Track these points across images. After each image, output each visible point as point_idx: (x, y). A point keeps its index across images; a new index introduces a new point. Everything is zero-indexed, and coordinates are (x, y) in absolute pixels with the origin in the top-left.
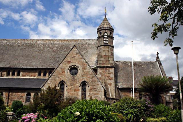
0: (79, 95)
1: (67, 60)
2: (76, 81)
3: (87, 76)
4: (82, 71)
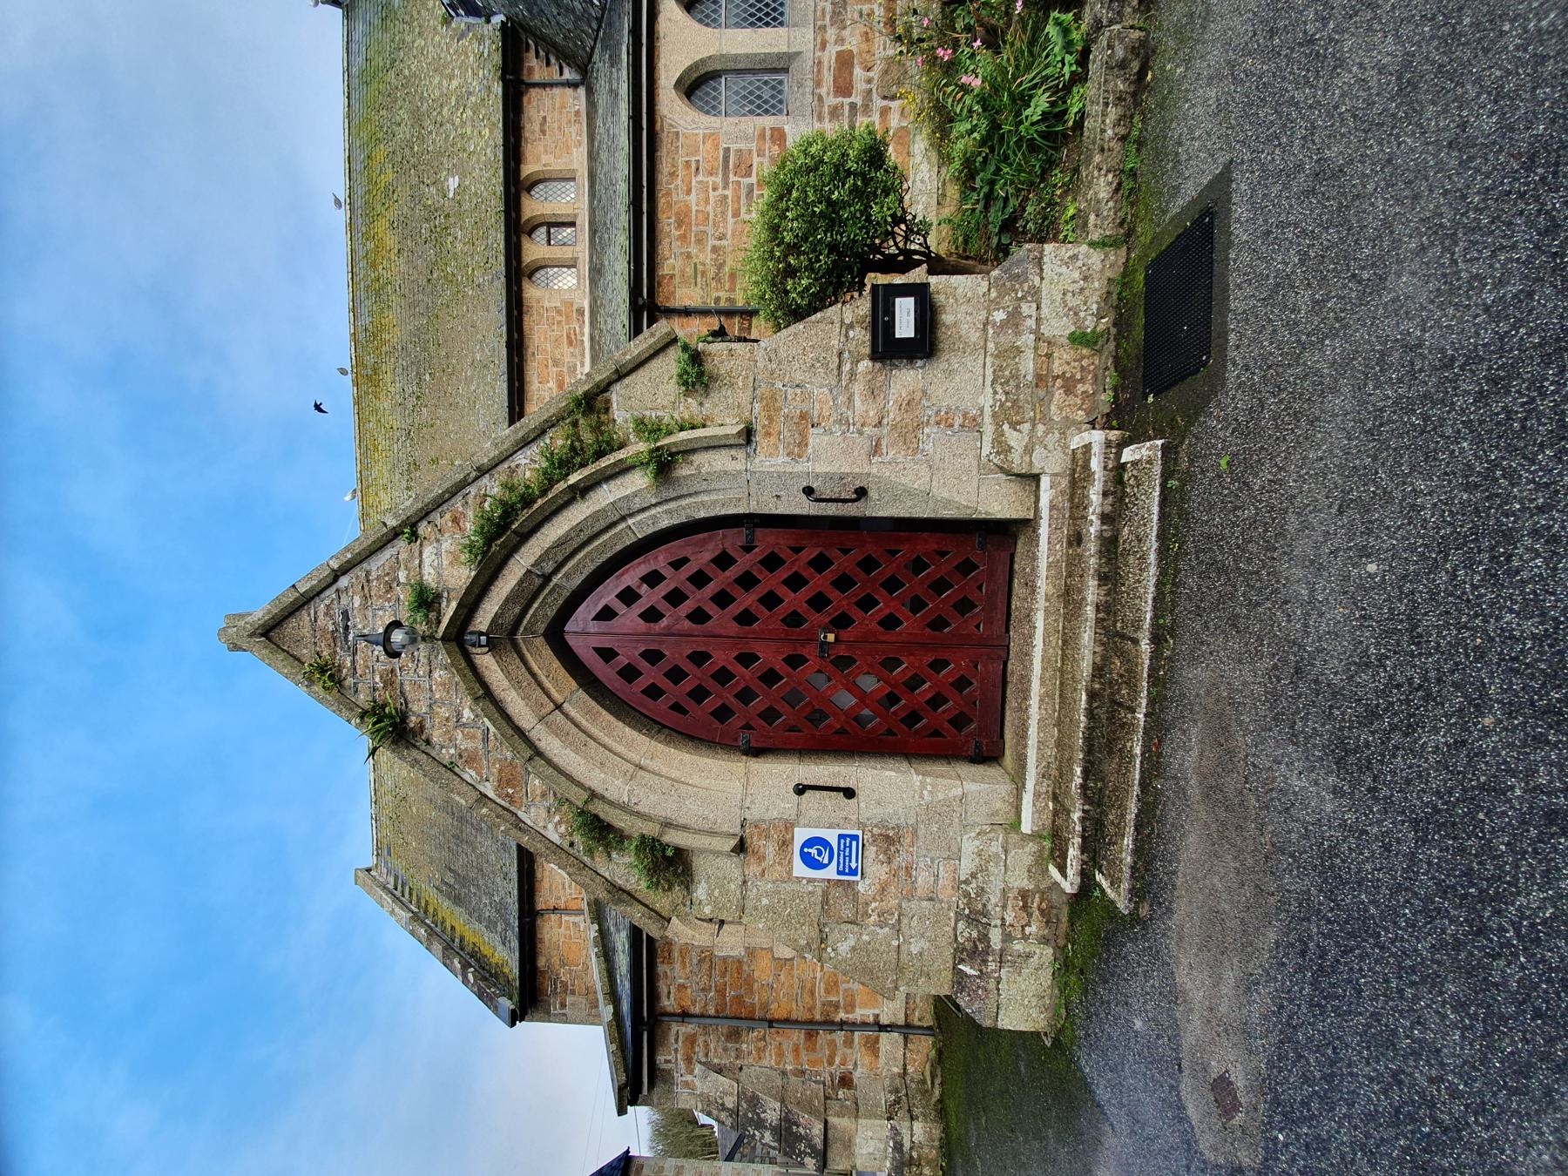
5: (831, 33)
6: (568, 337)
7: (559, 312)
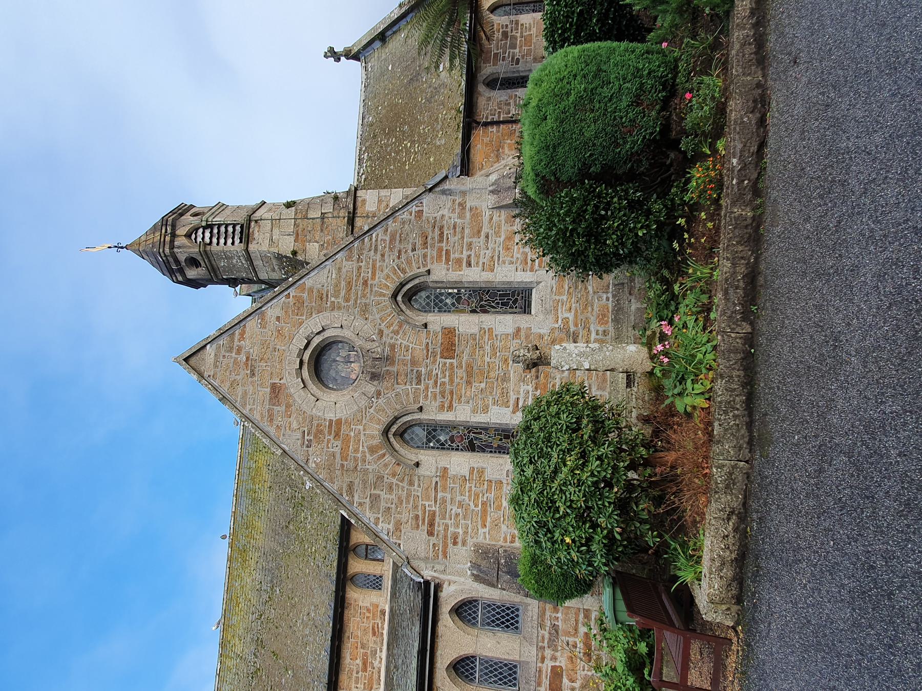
0: (498, 269)
1: (267, 402)
2: (392, 347)
3: (365, 283)
4: (335, 313)
5: (548, 653)
6: (373, 629)
7: (368, 610)
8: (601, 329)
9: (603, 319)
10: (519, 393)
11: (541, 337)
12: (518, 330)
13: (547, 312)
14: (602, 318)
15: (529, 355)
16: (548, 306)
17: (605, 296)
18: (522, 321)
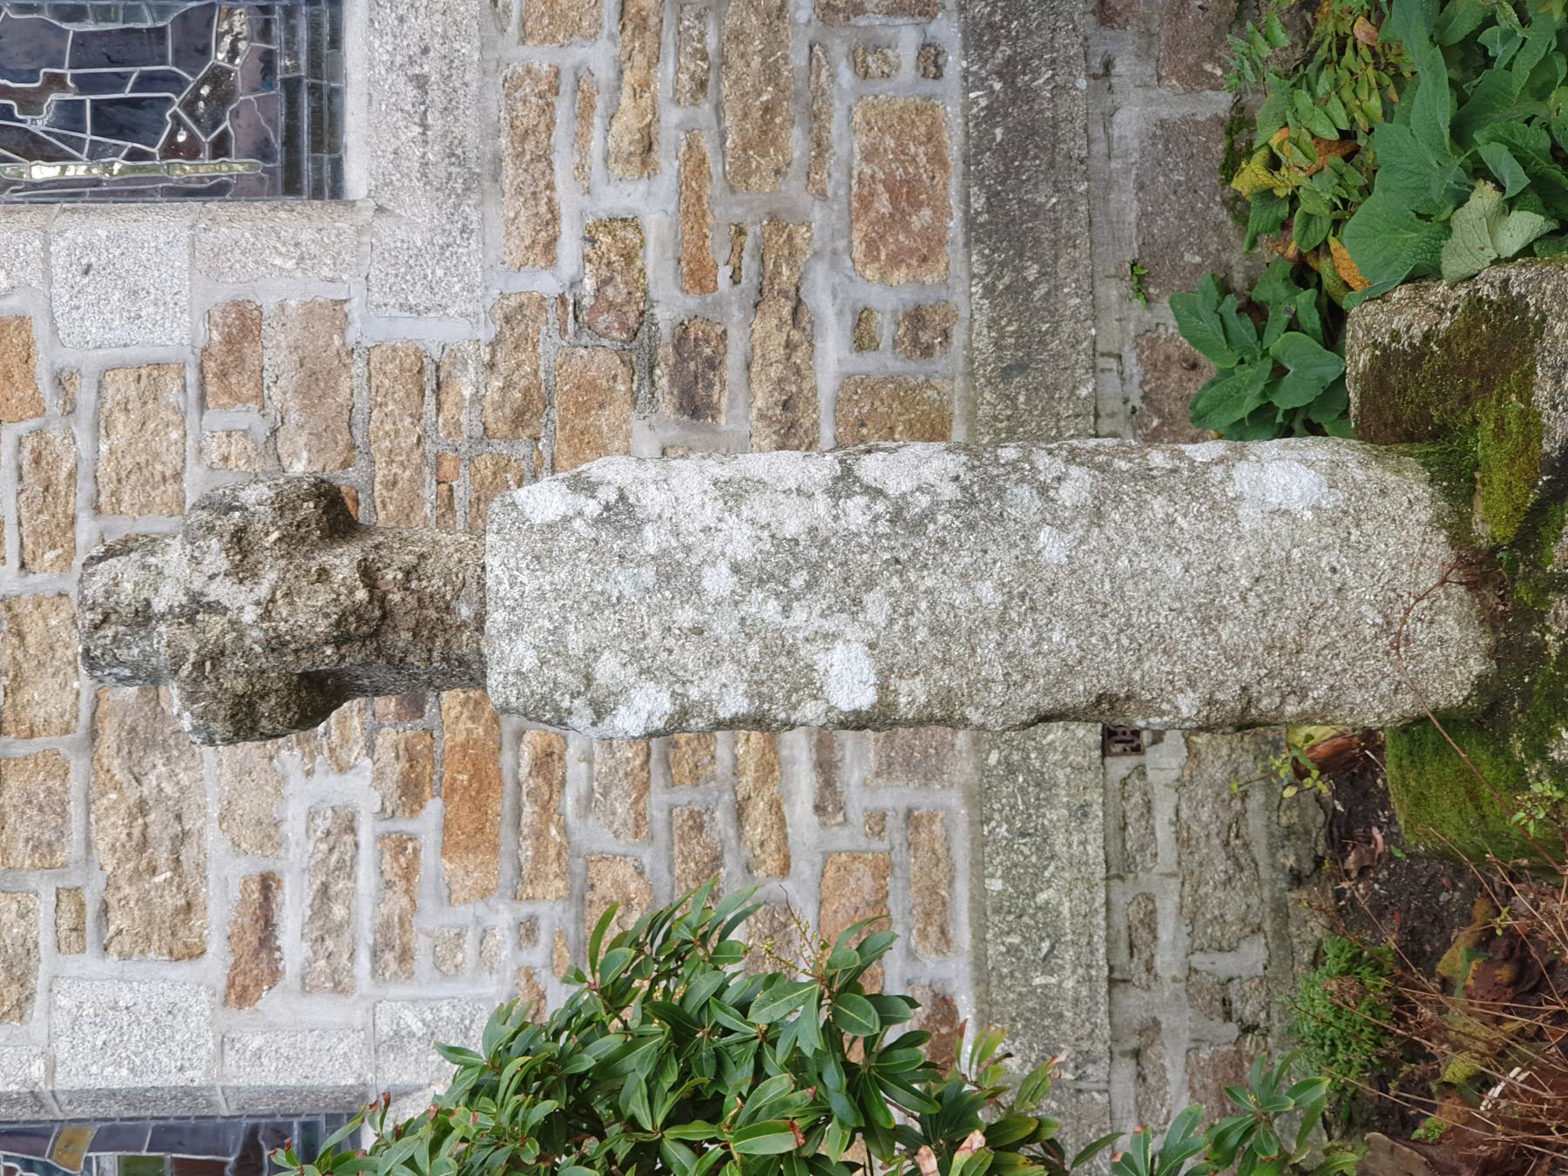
8: (889, 296)
9: (898, 218)
10: (269, 832)
11: (428, 377)
12: (243, 326)
13: (464, 177)
14: (892, 212)
15: (243, 600)
16: (468, 129)
17: (906, 39)
18: (270, 253)
